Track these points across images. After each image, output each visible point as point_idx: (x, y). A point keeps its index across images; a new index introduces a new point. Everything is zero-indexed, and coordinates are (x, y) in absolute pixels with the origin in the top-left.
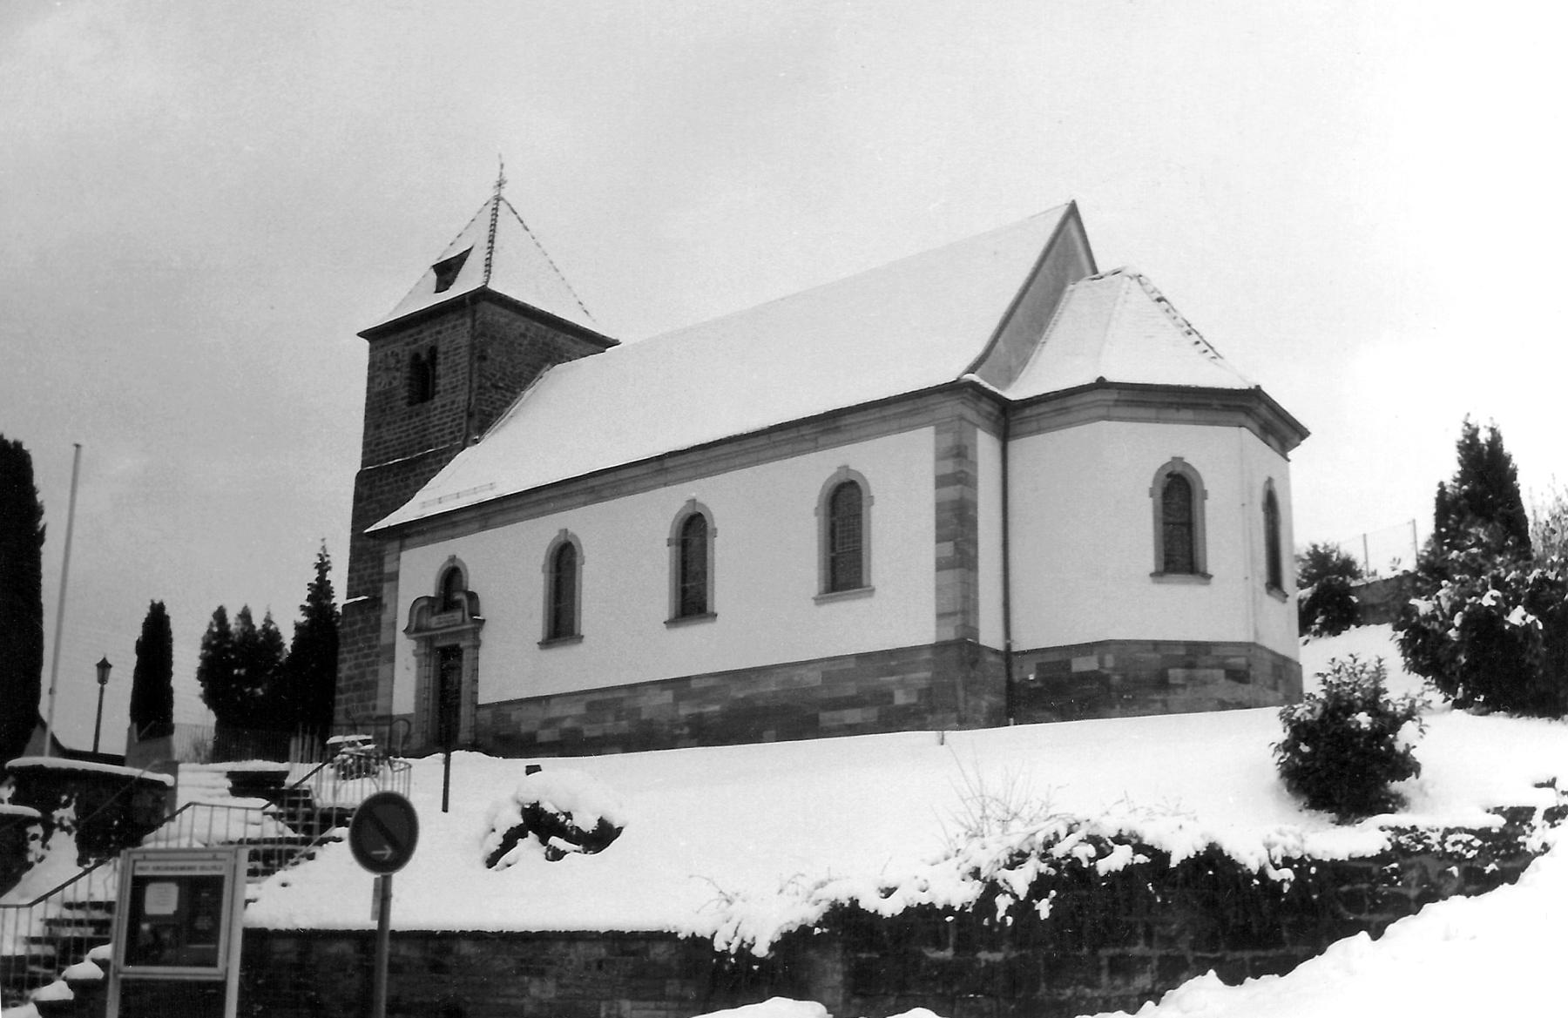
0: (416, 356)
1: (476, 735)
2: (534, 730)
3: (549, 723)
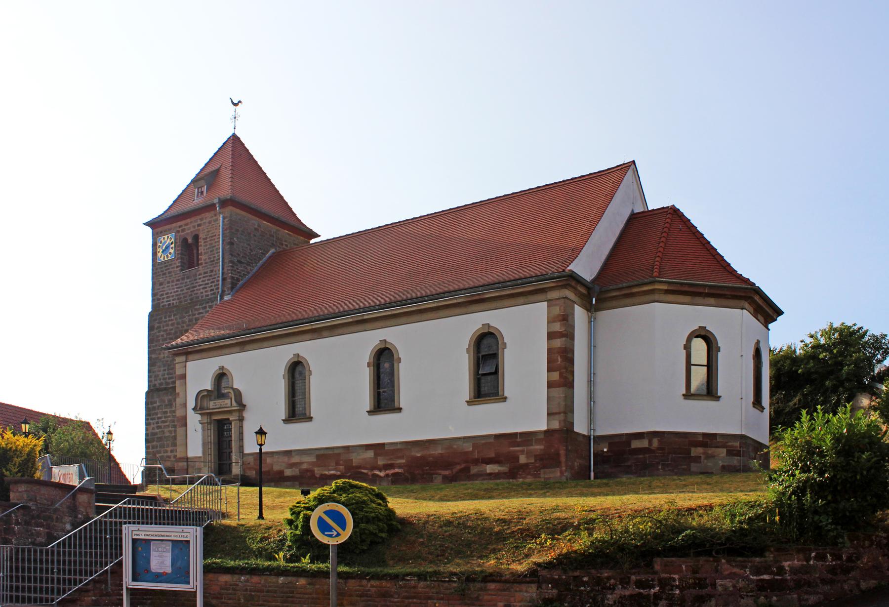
0: (185, 240)
1: (244, 470)
2: (282, 469)
3: (292, 466)
